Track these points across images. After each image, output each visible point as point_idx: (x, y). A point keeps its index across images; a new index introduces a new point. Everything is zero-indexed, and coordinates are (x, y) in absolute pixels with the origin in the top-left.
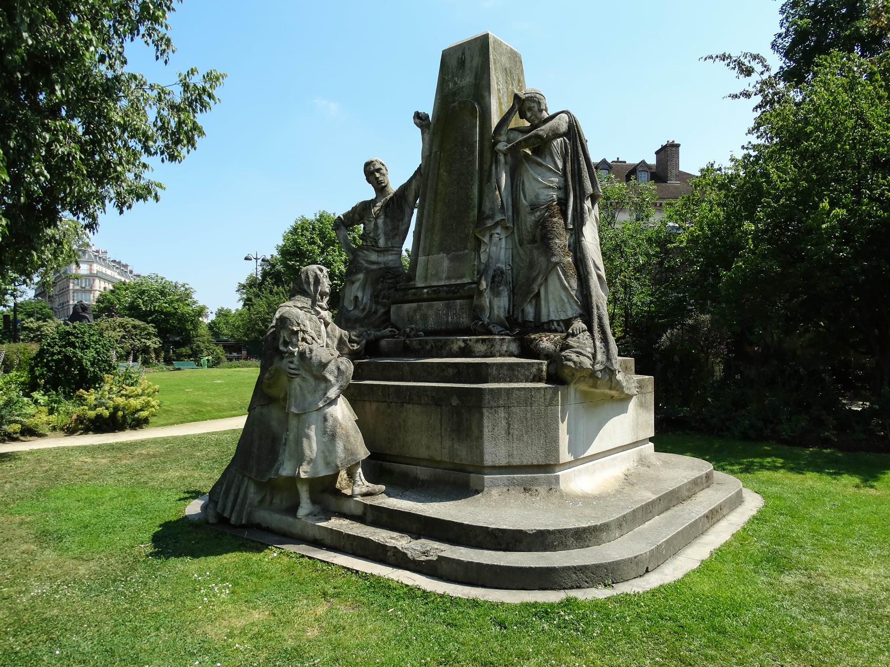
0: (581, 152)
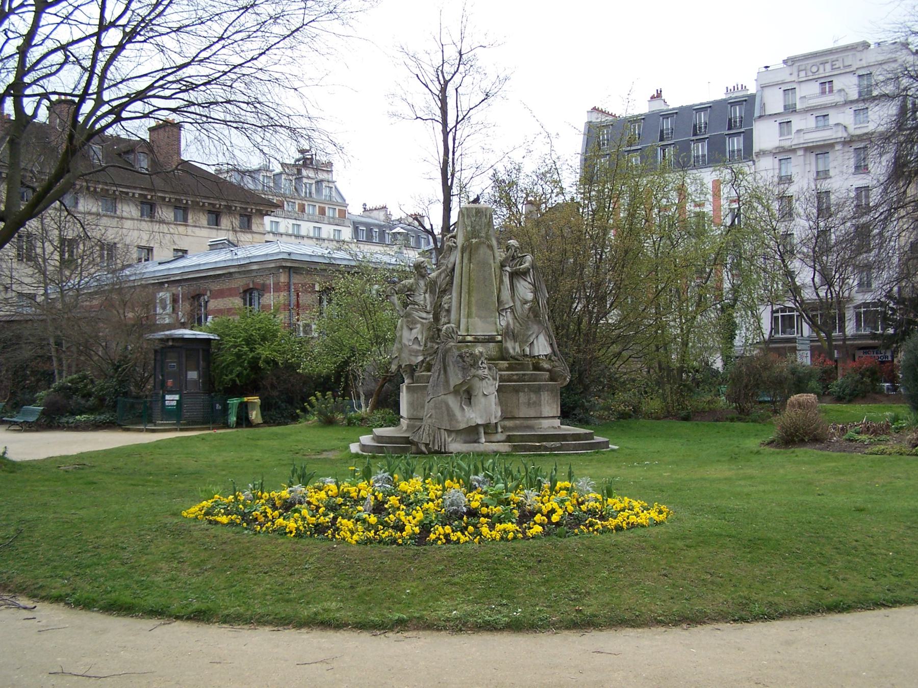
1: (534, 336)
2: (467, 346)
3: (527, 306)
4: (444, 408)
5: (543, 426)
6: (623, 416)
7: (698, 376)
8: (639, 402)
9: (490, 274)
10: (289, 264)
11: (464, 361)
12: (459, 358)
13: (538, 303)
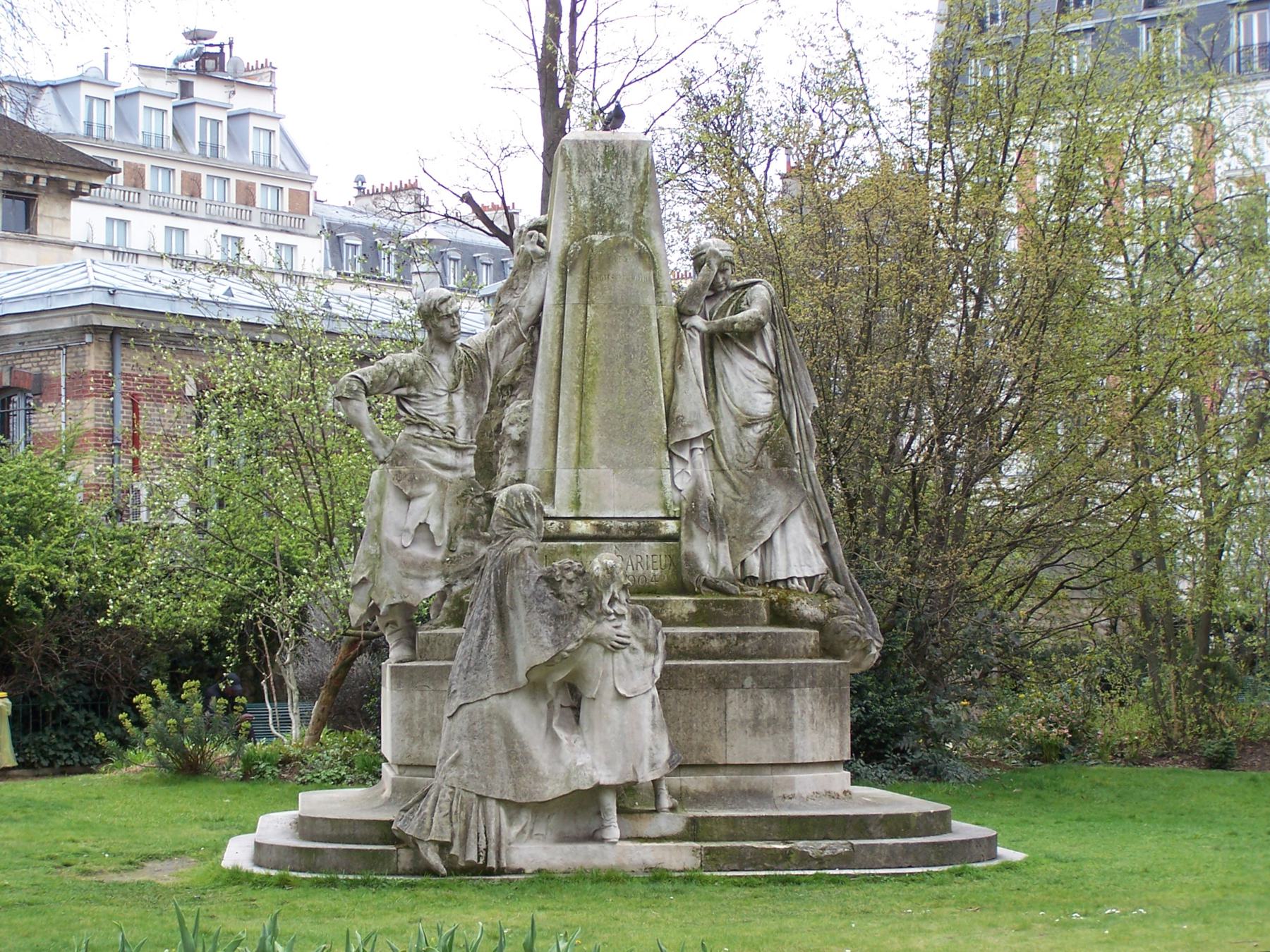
1: (774, 522)
2: (575, 551)
3: (753, 434)
4: (497, 738)
5: (799, 789)
6: (1043, 753)
7: (1253, 641)
8: (1086, 714)
9: (646, 335)
10: (109, 321)
11: (559, 596)
12: (544, 584)
13: (788, 424)
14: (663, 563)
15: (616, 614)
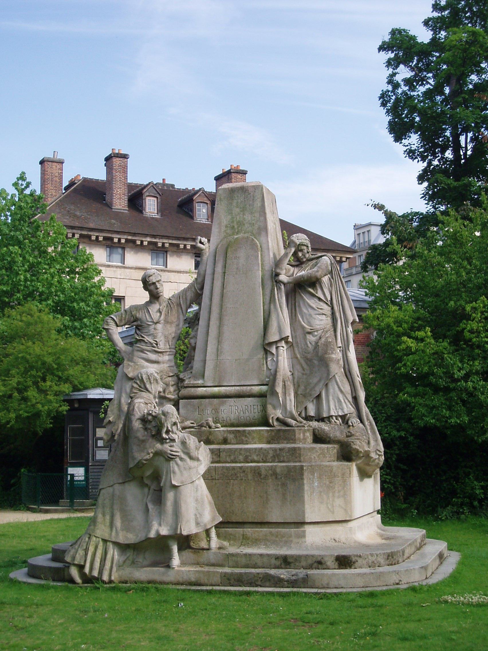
0: (83, 508)
14: (259, 409)
15: (169, 438)
